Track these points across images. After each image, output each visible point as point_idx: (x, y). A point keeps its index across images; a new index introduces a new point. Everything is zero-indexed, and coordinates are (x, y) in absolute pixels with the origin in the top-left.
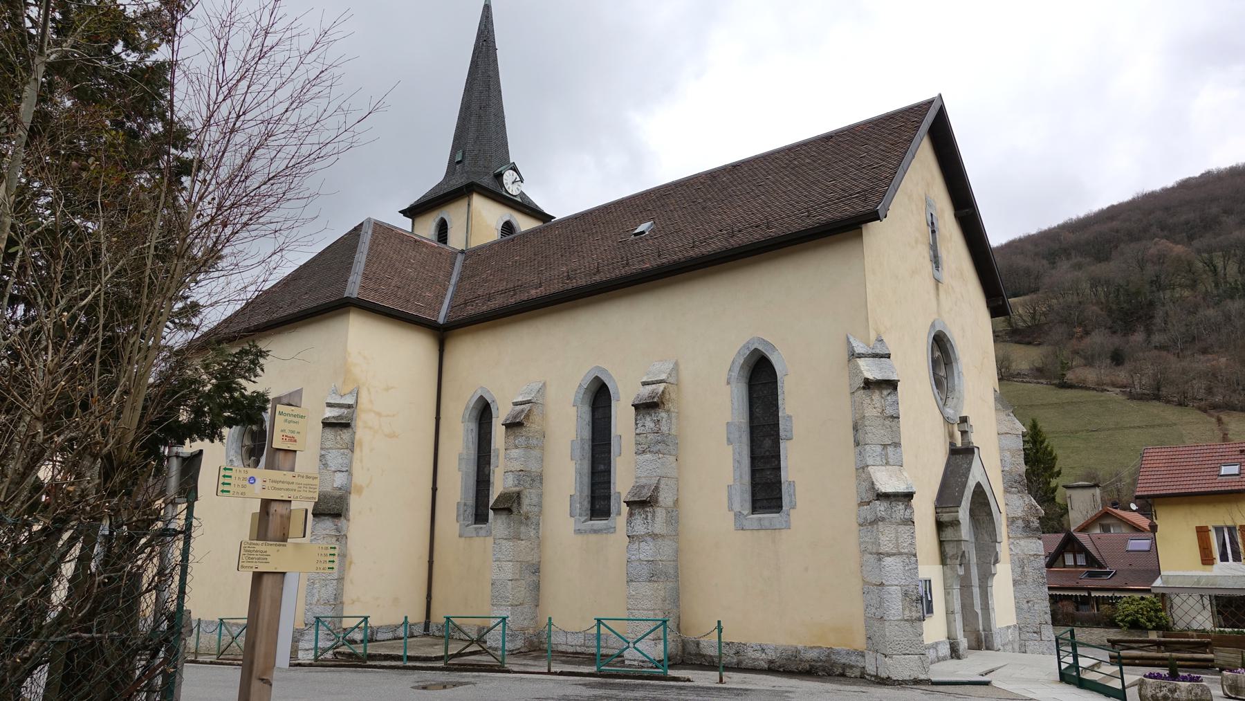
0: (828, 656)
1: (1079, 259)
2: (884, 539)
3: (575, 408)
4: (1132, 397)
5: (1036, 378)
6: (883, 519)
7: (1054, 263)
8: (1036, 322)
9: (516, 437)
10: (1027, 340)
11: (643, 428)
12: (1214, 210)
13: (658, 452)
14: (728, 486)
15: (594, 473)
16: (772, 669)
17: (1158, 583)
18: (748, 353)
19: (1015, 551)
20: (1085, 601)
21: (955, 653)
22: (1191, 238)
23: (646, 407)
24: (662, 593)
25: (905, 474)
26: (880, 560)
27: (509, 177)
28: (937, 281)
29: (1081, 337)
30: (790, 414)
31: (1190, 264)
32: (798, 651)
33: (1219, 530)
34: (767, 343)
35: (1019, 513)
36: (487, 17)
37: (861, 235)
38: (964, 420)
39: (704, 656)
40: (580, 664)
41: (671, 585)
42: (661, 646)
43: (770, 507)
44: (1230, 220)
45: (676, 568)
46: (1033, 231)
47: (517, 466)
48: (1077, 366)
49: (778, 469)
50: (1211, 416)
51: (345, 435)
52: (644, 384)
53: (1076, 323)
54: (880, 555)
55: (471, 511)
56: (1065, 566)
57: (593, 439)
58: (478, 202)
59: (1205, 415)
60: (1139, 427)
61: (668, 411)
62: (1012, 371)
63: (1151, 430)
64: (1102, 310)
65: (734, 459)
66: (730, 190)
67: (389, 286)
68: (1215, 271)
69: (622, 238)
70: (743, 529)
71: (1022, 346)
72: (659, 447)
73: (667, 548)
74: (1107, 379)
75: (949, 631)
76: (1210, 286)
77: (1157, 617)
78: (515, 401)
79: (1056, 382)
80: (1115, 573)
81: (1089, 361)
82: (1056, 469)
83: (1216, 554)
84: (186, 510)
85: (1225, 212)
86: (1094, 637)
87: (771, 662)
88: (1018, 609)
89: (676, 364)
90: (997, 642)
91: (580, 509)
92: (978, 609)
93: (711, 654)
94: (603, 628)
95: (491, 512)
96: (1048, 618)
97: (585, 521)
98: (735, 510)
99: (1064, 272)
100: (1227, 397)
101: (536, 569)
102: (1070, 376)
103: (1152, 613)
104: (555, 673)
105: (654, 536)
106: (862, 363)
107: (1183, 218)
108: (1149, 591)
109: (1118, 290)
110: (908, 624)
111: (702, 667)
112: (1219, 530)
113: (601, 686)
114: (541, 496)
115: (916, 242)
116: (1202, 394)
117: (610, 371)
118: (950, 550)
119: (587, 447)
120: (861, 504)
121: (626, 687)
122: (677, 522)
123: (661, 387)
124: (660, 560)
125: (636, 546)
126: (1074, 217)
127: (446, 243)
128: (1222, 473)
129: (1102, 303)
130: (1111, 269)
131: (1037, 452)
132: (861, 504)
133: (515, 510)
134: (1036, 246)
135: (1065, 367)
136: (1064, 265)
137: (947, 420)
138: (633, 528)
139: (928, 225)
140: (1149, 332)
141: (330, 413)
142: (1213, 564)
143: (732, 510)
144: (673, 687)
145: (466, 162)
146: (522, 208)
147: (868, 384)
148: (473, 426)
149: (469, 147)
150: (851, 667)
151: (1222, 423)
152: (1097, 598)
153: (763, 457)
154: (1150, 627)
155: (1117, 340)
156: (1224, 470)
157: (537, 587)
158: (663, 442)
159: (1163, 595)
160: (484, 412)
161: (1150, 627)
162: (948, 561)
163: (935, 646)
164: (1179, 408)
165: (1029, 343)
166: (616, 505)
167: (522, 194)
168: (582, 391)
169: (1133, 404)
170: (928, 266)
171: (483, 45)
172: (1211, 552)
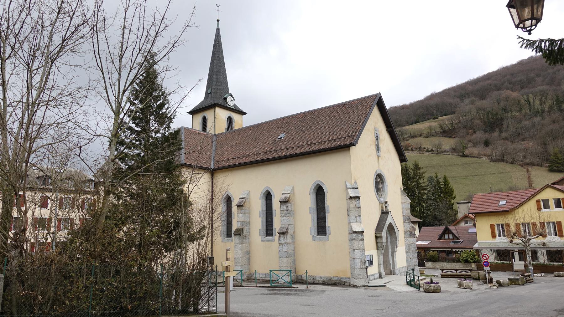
0: (340, 279)
1: (473, 98)
2: (355, 245)
4: (492, 160)
5: (452, 153)
6: (355, 239)
7: (463, 100)
8: (454, 127)
9: (241, 210)
10: (449, 135)
12: (532, 75)
13: (288, 217)
15: (267, 221)
16: (324, 284)
17: (476, 245)
19: (407, 242)
20: (451, 252)
21: (381, 277)
22: (522, 88)
23: (284, 202)
24: (290, 261)
25: (362, 225)
26: (354, 251)
27: (229, 99)
28: (378, 156)
29: (472, 134)
31: (519, 101)
32: (331, 278)
33: (498, 225)
34: (322, 182)
35: (408, 229)
36: (218, 33)
37: (350, 149)
38: (386, 203)
39: (303, 280)
40: (265, 283)
41: (293, 258)
42: (290, 278)
43: (323, 234)
44: (539, 80)
45: (294, 253)
46: (454, 85)
47: (241, 219)
48: (470, 147)
49: (325, 222)
50: (525, 168)
52: (283, 194)
53: (470, 128)
54: (354, 250)
55: (225, 233)
56: (445, 239)
57: (266, 210)
58: (218, 110)
59: (522, 168)
60: (494, 174)
61: (291, 203)
62: (442, 150)
63: (499, 175)
64: (481, 122)
65: (312, 219)
68: (530, 104)
70: (315, 241)
71: (447, 138)
72: (288, 215)
73: (291, 247)
74: (482, 153)
75: (379, 270)
76: (527, 111)
77: (474, 258)
78: (240, 197)
79: (461, 154)
80: (462, 242)
81: (475, 145)
82: (454, 196)
83: (497, 235)
85: (537, 76)
86: (453, 266)
87: (323, 281)
88: (407, 261)
89: (293, 187)
90: (397, 272)
92: (391, 262)
94: (272, 273)
96: (417, 263)
99: (466, 106)
100: (532, 160)
101: (249, 253)
102: (467, 152)
103: (473, 257)
104: (258, 287)
105: (287, 244)
106: (349, 191)
107: (519, 79)
108: (472, 248)
109: (488, 113)
110: (362, 270)
111: (303, 283)
112: (498, 225)
113: (272, 290)
114: (249, 229)
115: (371, 145)
116: (521, 158)
118: (379, 245)
119: (265, 213)
120: (349, 234)
121: (279, 290)
122: (294, 238)
123: (288, 195)
125: (281, 246)
126: (472, 78)
128: (500, 204)
129: (481, 119)
130: (485, 103)
131: (446, 189)
132: (349, 234)
133: (241, 234)
134: (455, 92)
135: (465, 148)
136: (467, 101)
137: (380, 203)
139: (375, 138)
140: (501, 131)
142: (495, 238)
144: (293, 290)
145: (213, 93)
146: (235, 111)
147: (351, 198)
149: (213, 87)
150: (346, 282)
151: (529, 171)
152: (455, 251)
153: (321, 218)
154: (472, 262)
155: (487, 136)
156: (501, 203)
157: (249, 259)
158: (289, 213)
159: (477, 250)
160: (229, 200)
161: (472, 262)
162: (379, 248)
163: (374, 275)
164: (512, 165)
165: (450, 137)
167: (235, 105)
169: (492, 163)
170: (375, 152)
172: (495, 234)
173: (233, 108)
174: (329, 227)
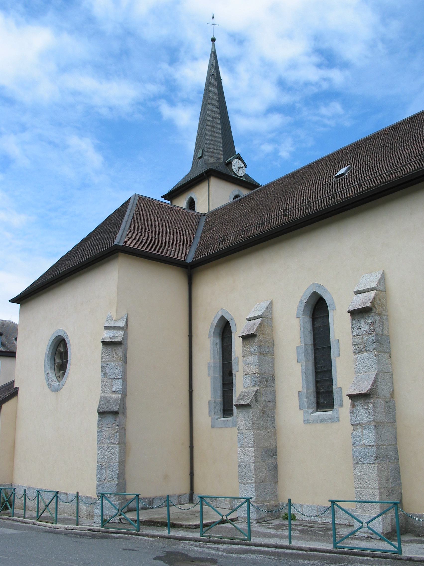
3: (298, 320)
27: (236, 164)
45: (396, 451)
51: (119, 351)
52: (357, 293)
55: (219, 407)
57: (315, 344)
58: (214, 183)
66: (412, 133)
67: (149, 237)
69: (325, 182)
78: (248, 317)
84: (373, 293)
91: (308, 402)
94: (339, 513)
95: (235, 408)
97: (312, 413)
124: (382, 445)
127: (194, 210)
133: (355, 354)
138: (356, 417)
141: (108, 335)
148: (218, 340)
157: (275, 468)
166: (339, 398)
167: (246, 176)
168: (303, 305)
171: (212, 78)
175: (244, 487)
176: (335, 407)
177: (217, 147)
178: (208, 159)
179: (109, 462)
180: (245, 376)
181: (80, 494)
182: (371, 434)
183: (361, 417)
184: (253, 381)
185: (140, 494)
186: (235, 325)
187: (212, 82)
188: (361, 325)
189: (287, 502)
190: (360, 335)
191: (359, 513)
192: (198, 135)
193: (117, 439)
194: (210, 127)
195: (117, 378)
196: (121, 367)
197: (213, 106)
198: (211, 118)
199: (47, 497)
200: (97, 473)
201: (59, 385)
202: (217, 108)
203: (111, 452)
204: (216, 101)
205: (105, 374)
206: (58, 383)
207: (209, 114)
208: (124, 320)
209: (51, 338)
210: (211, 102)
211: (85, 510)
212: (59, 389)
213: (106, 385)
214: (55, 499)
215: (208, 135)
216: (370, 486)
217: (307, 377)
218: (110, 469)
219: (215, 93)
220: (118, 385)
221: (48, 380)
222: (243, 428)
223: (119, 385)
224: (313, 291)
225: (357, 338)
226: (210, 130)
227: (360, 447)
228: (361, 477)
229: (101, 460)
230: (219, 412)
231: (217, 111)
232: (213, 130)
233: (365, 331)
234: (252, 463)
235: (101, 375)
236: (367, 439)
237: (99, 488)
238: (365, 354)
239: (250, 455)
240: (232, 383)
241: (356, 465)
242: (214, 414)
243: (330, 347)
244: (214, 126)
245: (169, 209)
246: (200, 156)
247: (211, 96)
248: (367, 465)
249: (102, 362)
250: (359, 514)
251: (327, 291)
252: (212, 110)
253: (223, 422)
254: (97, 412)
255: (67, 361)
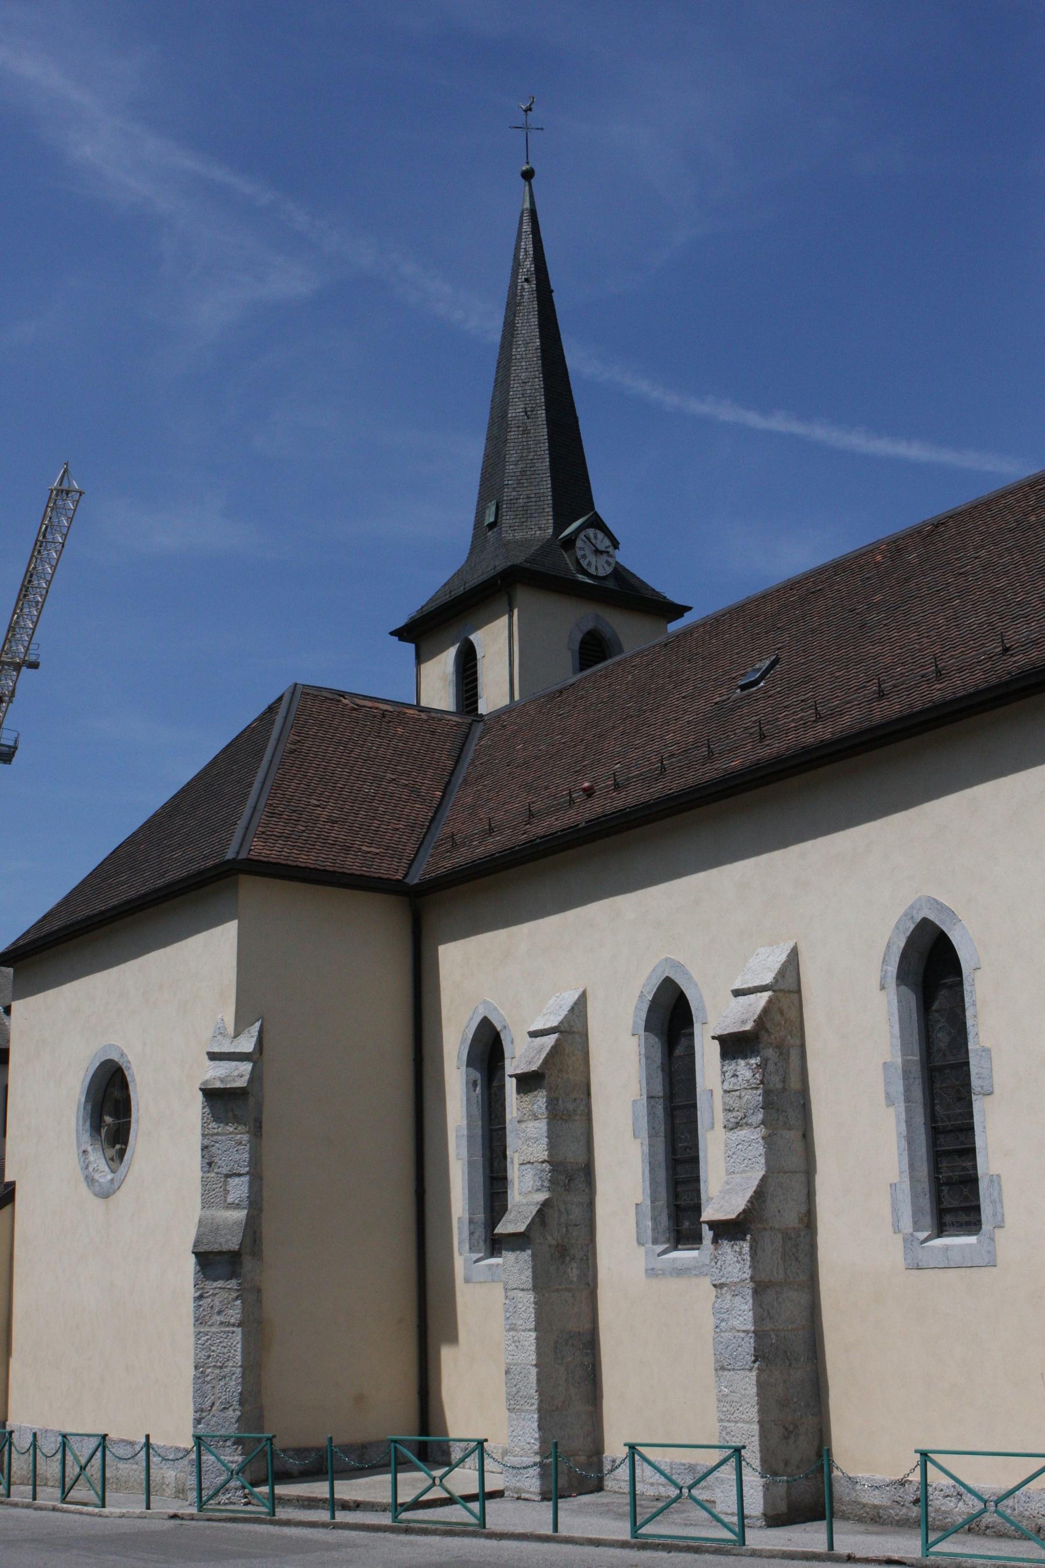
3: (636, 1038)
11: (733, 1080)
14: (891, 1185)
18: (912, 927)
30: (987, 1045)
34: (942, 908)
52: (737, 993)
78: (533, 1028)
84: (766, 996)
91: (653, 1230)
93: (876, 1502)
94: (644, 1472)
97: (664, 1252)
98: (905, 1231)
117: (689, 968)
138: (721, 1270)
141: (217, 1074)
143: (899, 1231)
149: (508, 494)
167: (620, 574)
173: (611, 584)
174: (996, 1180)
175: (517, 1419)
176: (703, 1241)
177: (537, 495)
178: (511, 529)
179: (221, 1368)
180: (523, 1167)
181: (151, 1441)
182: (746, 1307)
183: (729, 1269)
184: (538, 1179)
185: (486, 1440)
186: (512, 1042)
187: (523, 302)
188: (739, 1068)
189: (144, 1440)
190: (736, 1090)
191: (725, 1474)
192: (488, 456)
193: (238, 1314)
194: (517, 437)
195: (237, 1172)
196: (247, 1148)
197: (527, 374)
198: (521, 410)
199: (84, 1449)
200: (194, 1392)
201: (112, 1180)
202: (537, 380)
203: (225, 1345)
204: (535, 359)
205: (209, 1164)
206: (110, 1176)
207: (515, 396)
208: (252, 1037)
209: (91, 1064)
210: (521, 360)
211: (174, 1479)
212: (111, 1191)
213: (214, 1190)
214: (99, 1454)
215: (513, 459)
216: (743, 1416)
217: (652, 1170)
218: (222, 1383)
219: (532, 334)
220: (241, 1190)
221: (87, 1167)
222: (515, 1286)
223: (242, 1188)
224: (664, 977)
225: (731, 1095)
226: (517, 444)
227: (727, 1334)
228: (728, 1399)
229: (203, 1362)
230: (482, 1244)
231: (537, 387)
232: (528, 445)
233: (744, 1082)
234: (532, 1365)
235: (202, 1167)
236: (740, 1318)
237: (200, 1426)
238: (745, 1131)
239: (529, 1348)
240: (505, 1178)
241: (720, 1373)
242: (470, 1249)
243: (694, 1106)
244: (530, 433)
245: (384, 716)
246: (492, 519)
247: (520, 342)
248: (739, 1372)
249: (203, 1135)
250: (723, 1475)
251: (692, 977)
252: (524, 384)
253: (487, 1268)
254: (193, 1253)
255: (130, 1122)
